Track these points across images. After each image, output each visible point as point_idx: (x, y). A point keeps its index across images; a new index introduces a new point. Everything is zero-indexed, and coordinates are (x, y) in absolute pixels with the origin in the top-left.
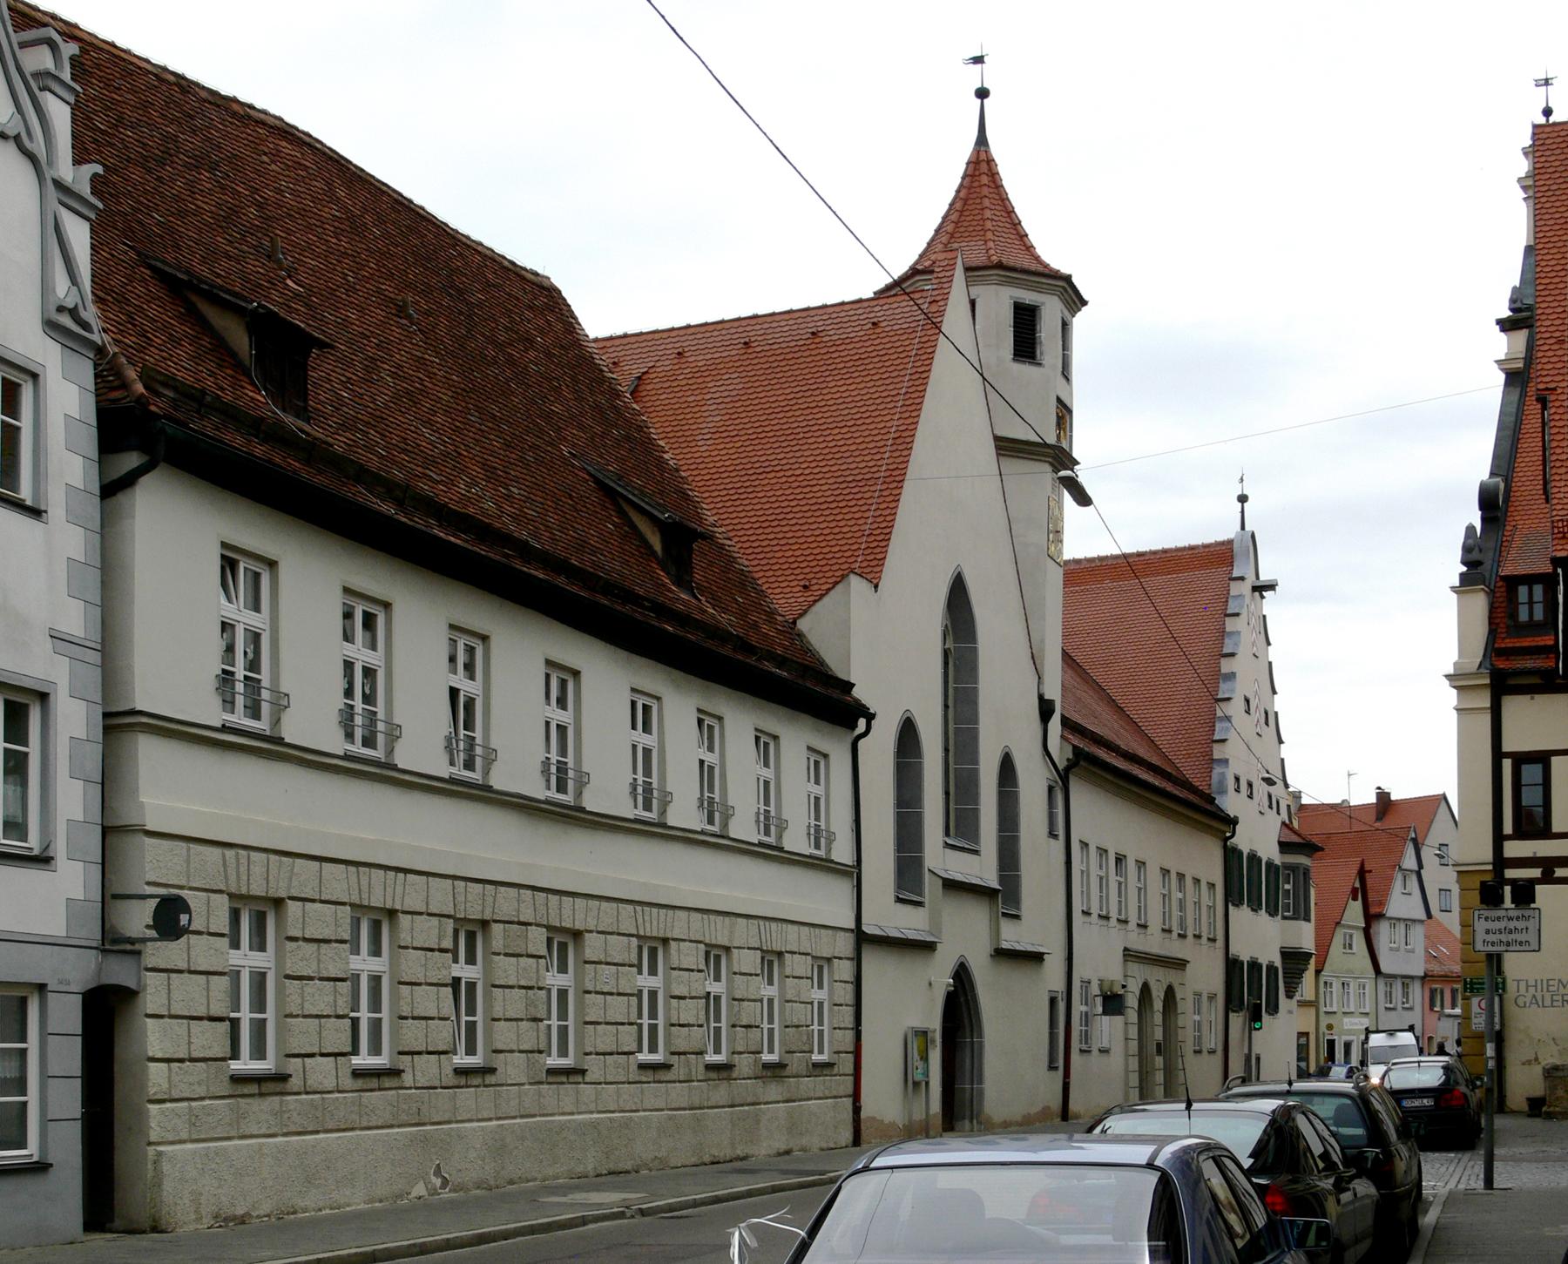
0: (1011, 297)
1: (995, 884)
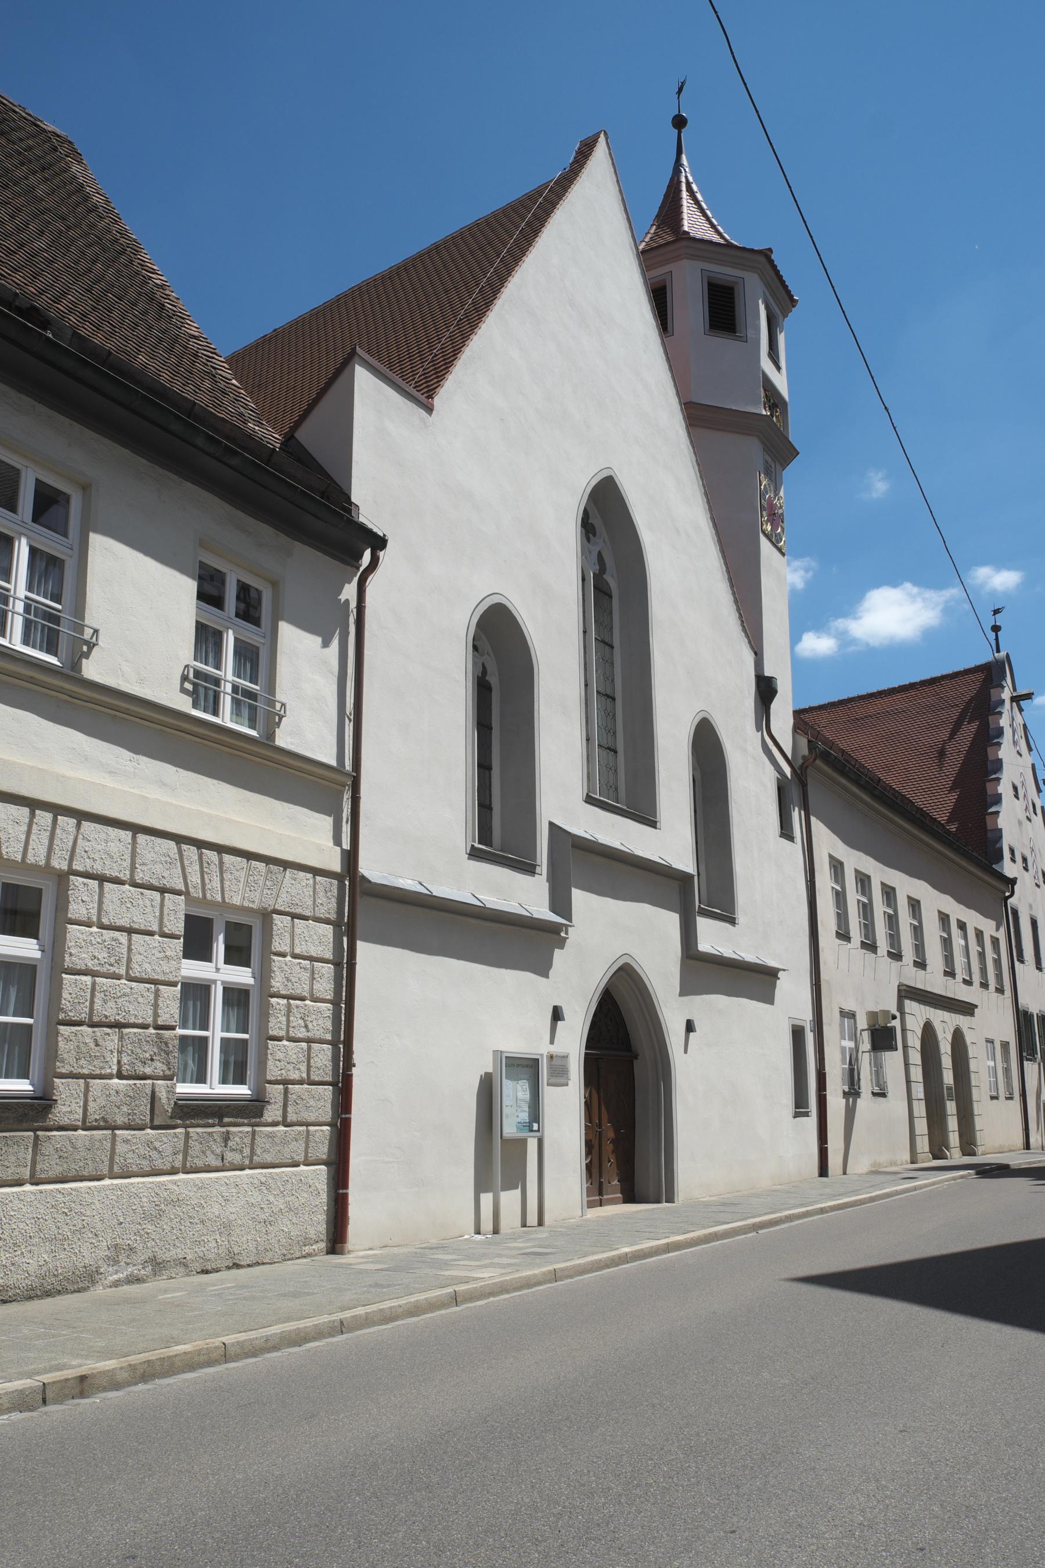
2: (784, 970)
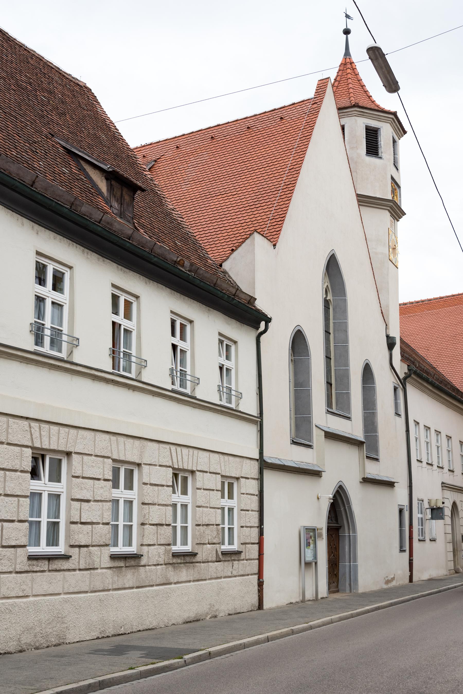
0: (364, 123)
1: (362, 438)
2: (397, 483)
